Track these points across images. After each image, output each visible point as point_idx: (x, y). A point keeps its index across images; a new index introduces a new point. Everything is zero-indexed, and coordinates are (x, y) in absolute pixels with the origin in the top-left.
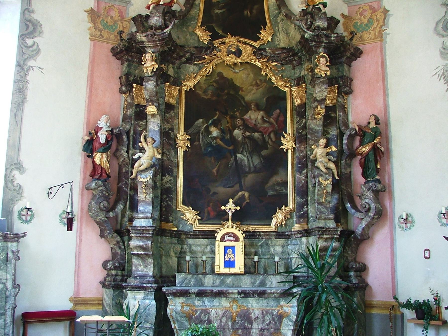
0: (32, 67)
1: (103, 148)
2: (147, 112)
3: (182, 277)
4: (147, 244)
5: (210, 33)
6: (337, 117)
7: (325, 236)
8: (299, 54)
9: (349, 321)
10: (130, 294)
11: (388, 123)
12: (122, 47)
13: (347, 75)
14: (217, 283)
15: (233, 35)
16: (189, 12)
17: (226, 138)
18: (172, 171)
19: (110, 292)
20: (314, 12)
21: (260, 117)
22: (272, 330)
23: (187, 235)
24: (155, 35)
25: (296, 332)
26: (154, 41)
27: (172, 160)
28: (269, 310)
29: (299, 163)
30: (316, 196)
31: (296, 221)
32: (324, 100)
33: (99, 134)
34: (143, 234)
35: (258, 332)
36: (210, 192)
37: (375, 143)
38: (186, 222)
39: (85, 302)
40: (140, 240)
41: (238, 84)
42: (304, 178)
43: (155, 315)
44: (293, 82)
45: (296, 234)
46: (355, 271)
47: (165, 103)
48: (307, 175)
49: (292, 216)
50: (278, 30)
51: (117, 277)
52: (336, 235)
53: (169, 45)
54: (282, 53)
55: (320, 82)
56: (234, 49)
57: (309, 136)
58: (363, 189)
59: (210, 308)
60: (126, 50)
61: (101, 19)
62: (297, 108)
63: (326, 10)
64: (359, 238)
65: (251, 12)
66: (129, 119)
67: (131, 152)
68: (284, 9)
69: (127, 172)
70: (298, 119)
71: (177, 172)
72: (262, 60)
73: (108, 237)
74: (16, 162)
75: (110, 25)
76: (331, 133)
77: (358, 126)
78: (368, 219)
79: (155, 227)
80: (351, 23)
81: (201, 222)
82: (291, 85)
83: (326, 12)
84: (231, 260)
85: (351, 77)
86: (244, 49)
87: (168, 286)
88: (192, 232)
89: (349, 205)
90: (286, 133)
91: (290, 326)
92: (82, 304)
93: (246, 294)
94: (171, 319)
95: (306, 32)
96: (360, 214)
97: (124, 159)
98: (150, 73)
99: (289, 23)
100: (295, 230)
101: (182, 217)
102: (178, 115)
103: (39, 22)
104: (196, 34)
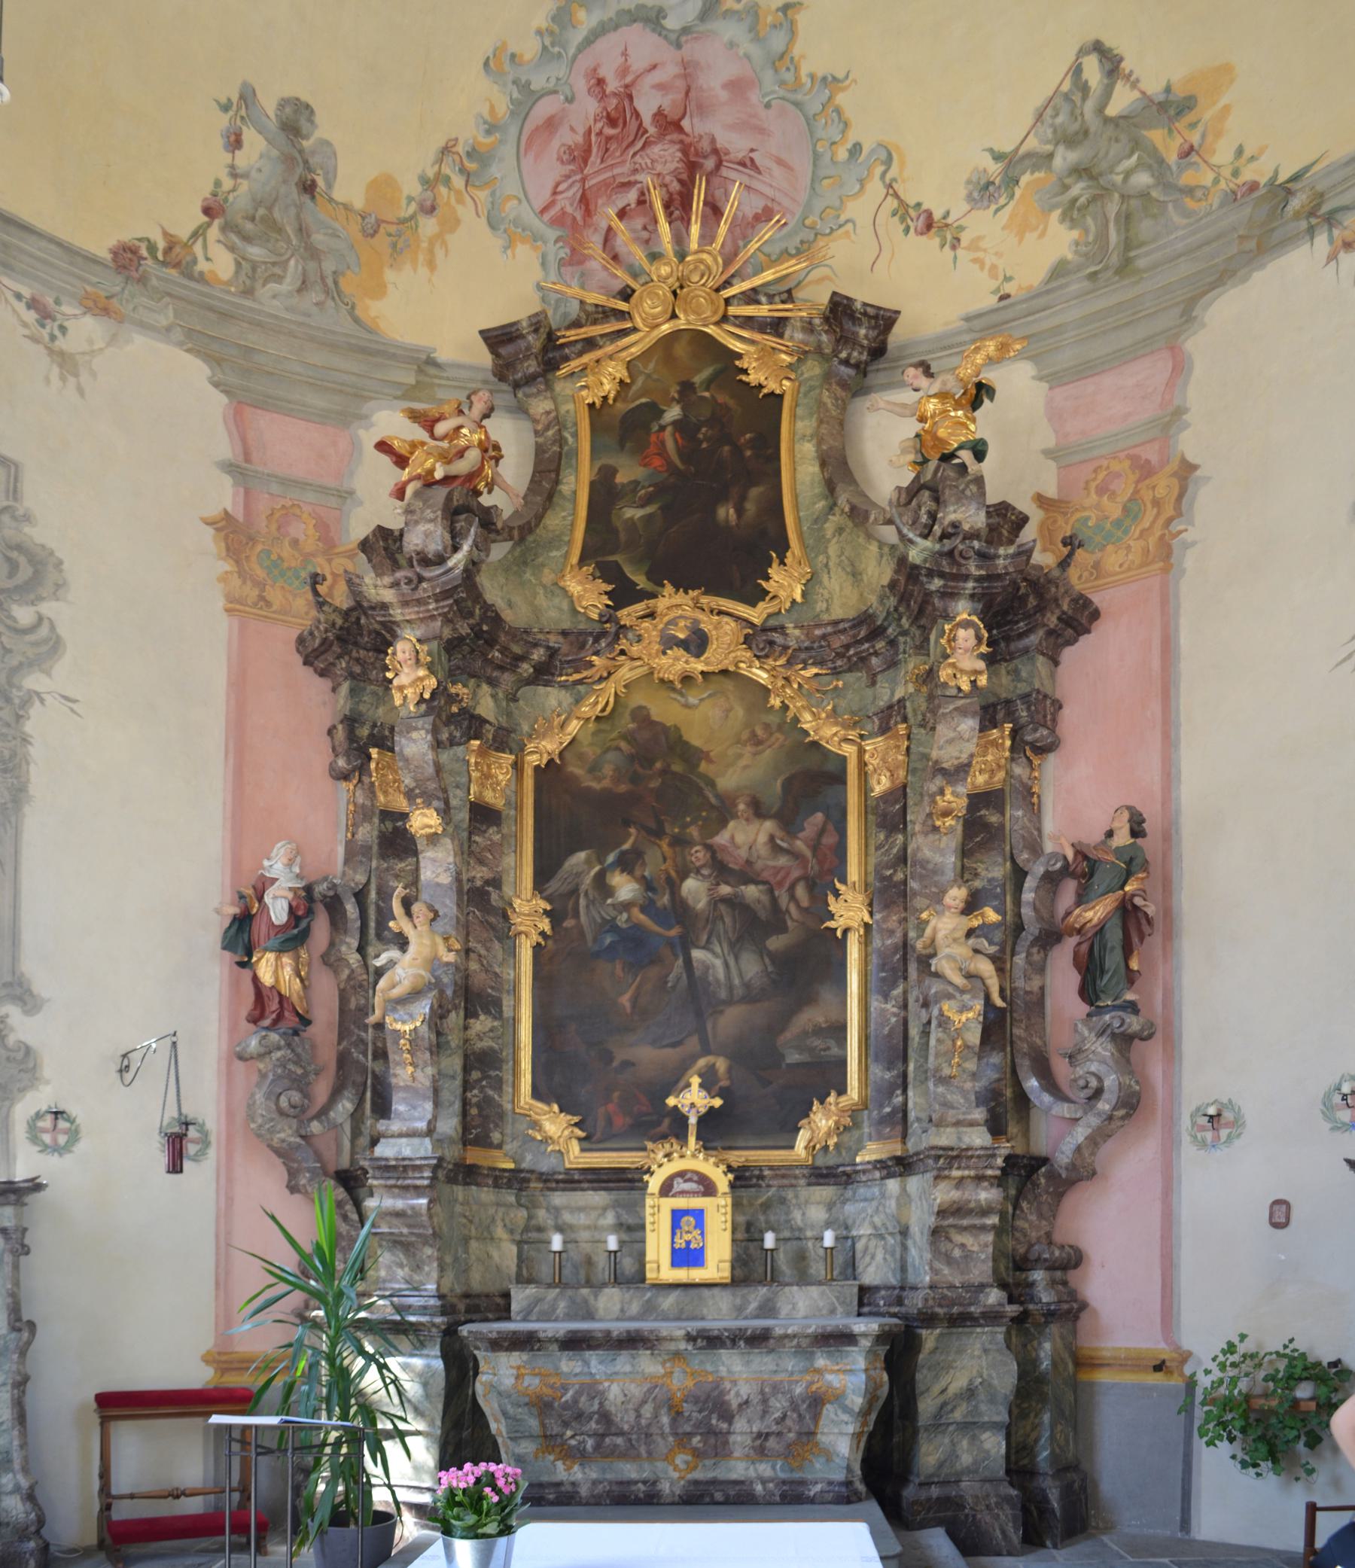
0: (38, 694)
1: (281, 937)
5: (609, 583)
7: (956, 1173)
8: (890, 630)
9: (1025, 1405)
11: (1173, 831)
13: (1048, 690)
14: (635, 1308)
15: (682, 584)
16: (539, 518)
17: (659, 904)
18: (497, 1003)
20: (944, 479)
21: (762, 838)
22: (792, 1435)
24: (421, 579)
26: (419, 602)
27: (496, 974)
28: (781, 1382)
29: (882, 967)
30: (931, 1058)
31: (870, 1134)
32: (962, 770)
33: (267, 899)
34: (405, 1178)
35: (749, 1442)
37: (1125, 893)
38: (543, 1147)
40: (394, 1197)
41: (696, 741)
42: (895, 1010)
43: (442, 1399)
46: (1048, 1269)
50: (827, 565)
52: (992, 1168)
54: (835, 633)
55: (956, 709)
57: (913, 885)
60: (338, 638)
61: (259, 548)
62: (877, 806)
63: (987, 467)
64: (1064, 1176)
65: (740, 511)
66: (363, 855)
67: (371, 950)
70: (882, 836)
72: (771, 662)
74: (8, 978)
75: (289, 568)
76: (984, 873)
77: (1073, 845)
78: (1094, 1121)
81: (586, 1145)
82: (862, 737)
83: (982, 477)
84: (693, 1246)
85: (1058, 695)
86: (716, 628)
90: (844, 881)
91: (843, 1426)
93: (712, 1341)
95: (911, 541)
97: (353, 971)
99: (861, 540)
100: (867, 1158)
103: (52, 553)
104: (564, 590)
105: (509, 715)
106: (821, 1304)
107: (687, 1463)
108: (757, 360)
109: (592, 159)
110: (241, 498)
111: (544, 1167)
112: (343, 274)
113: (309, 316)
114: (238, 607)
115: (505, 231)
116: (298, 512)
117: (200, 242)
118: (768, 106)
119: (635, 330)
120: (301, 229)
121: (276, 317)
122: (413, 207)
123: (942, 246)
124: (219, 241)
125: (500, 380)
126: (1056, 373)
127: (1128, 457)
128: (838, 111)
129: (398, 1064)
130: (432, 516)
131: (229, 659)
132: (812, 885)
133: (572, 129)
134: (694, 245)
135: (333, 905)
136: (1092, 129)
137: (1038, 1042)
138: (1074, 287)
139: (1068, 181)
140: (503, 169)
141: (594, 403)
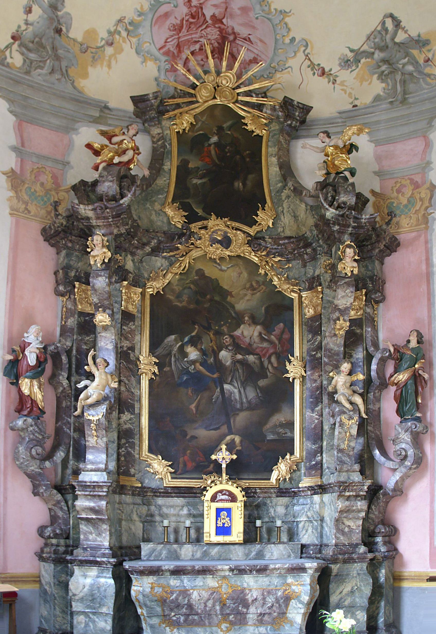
2: (96, 323)
3: (149, 549)
4: (101, 506)
5: (186, 212)
6: (364, 334)
7: (347, 494)
8: (314, 244)
10: (77, 571)
12: (58, 227)
14: (198, 555)
15: (220, 215)
17: (209, 362)
18: (133, 407)
19: (50, 567)
21: (256, 334)
22: (275, 614)
23: (154, 492)
25: (307, 615)
26: (105, 218)
27: (132, 392)
28: (272, 590)
30: (336, 441)
31: (305, 473)
33: (27, 352)
34: (94, 491)
35: (256, 617)
36: (186, 435)
38: (153, 476)
39: (16, 579)
40: (88, 500)
41: (225, 287)
42: (317, 417)
43: (114, 598)
44: (303, 286)
45: (305, 491)
47: (122, 310)
48: (322, 412)
49: (300, 467)
51: (59, 548)
53: (127, 224)
55: (345, 283)
56: (219, 237)
58: (398, 431)
59: (192, 589)
61: (26, 186)
65: (244, 184)
67: (73, 379)
68: (291, 181)
69: (68, 407)
70: (310, 337)
71: (140, 409)
72: (259, 253)
73: (45, 495)
75: (39, 196)
78: (403, 470)
79: (112, 483)
80: (384, 204)
81: (174, 476)
82: (300, 290)
84: (226, 525)
86: (235, 236)
87: (131, 560)
88: (162, 489)
89: (377, 453)
91: (299, 609)
92: (11, 581)
94: (137, 604)
95: (327, 209)
96: (393, 464)
97: (64, 388)
98: (99, 265)
101: (148, 469)
102: (141, 328)
104: (165, 212)
105: (139, 269)
106: (284, 553)
107: (227, 627)
108: (251, 120)
109: (183, 30)
110: (19, 164)
111: (153, 485)
112: (70, 68)
113: (54, 84)
114: (15, 213)
115: (143, 55)
116: (44, 170)
117: (9, 50)
118: (257, 18)
119: (197, 102)
120: (53, 48)
121: (39, 84)
122: (103, 42)
123: (329, 82)
124: (17, 51)
125: (137, 117)
126: (377, 140)
127: (409, 179)
128: (286, 24)
129: (89, 435)
130: (111, 179)
131: (10, 237)
132: (278, 358)
133: (176, 18)
134: (224, 69)
135: (56, 356)
136: (390, 46)
137: (378, 433)
138: (384, 106)
139: (380, 64)
140: (144, 31)
141: (179, 132)
